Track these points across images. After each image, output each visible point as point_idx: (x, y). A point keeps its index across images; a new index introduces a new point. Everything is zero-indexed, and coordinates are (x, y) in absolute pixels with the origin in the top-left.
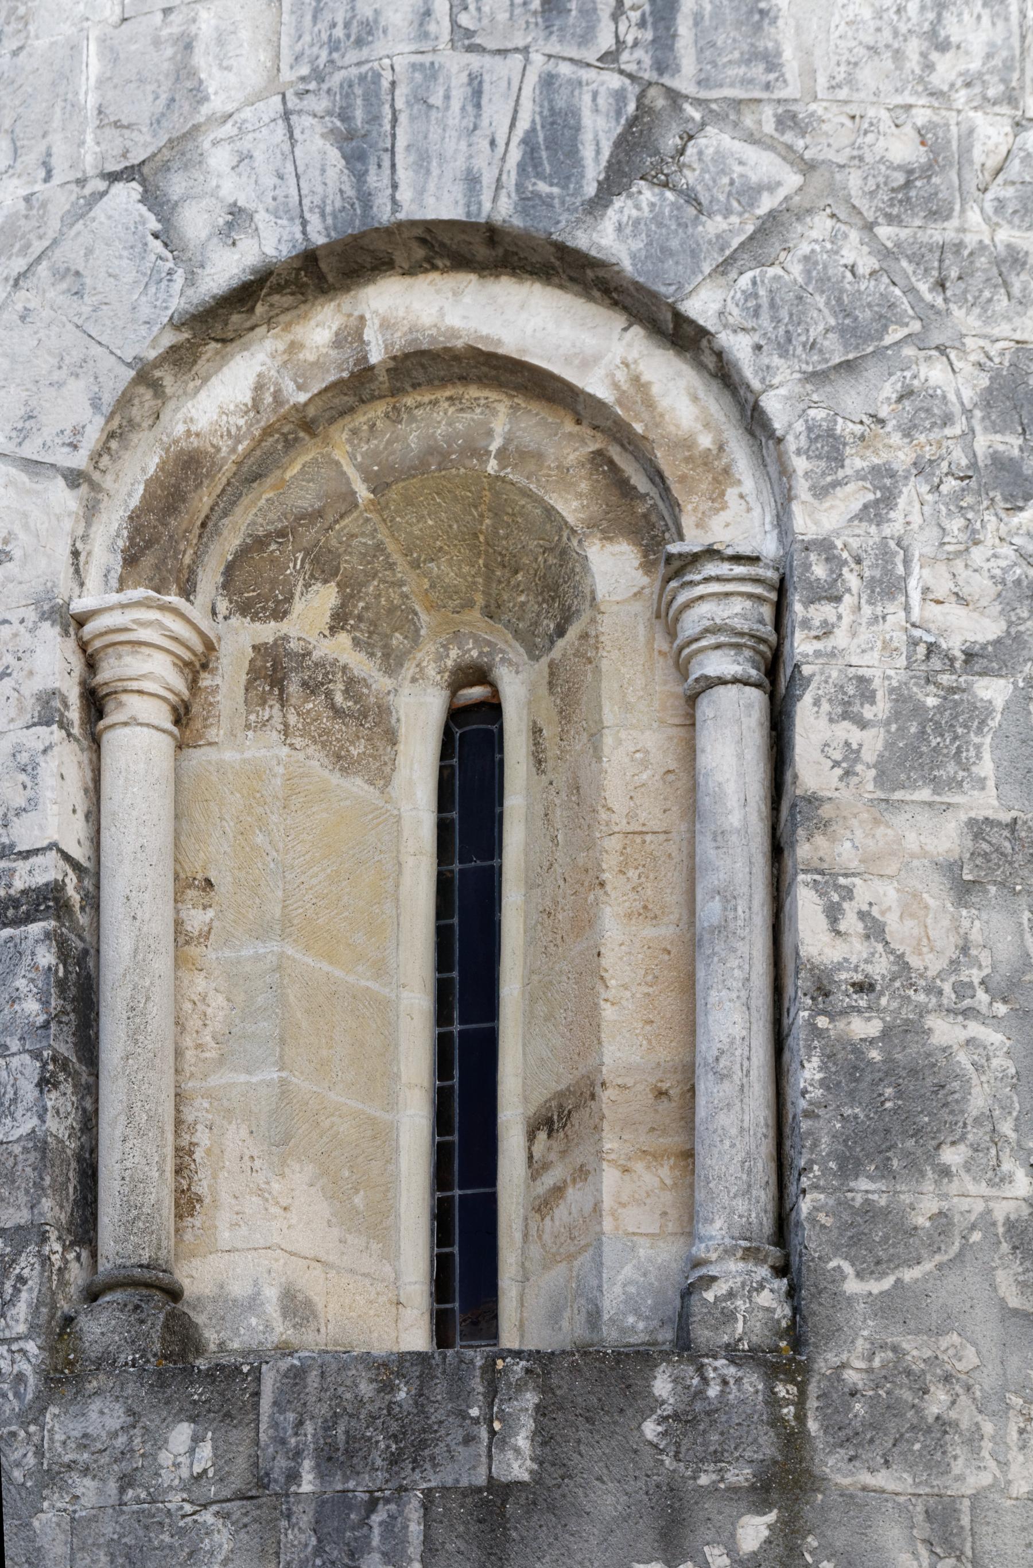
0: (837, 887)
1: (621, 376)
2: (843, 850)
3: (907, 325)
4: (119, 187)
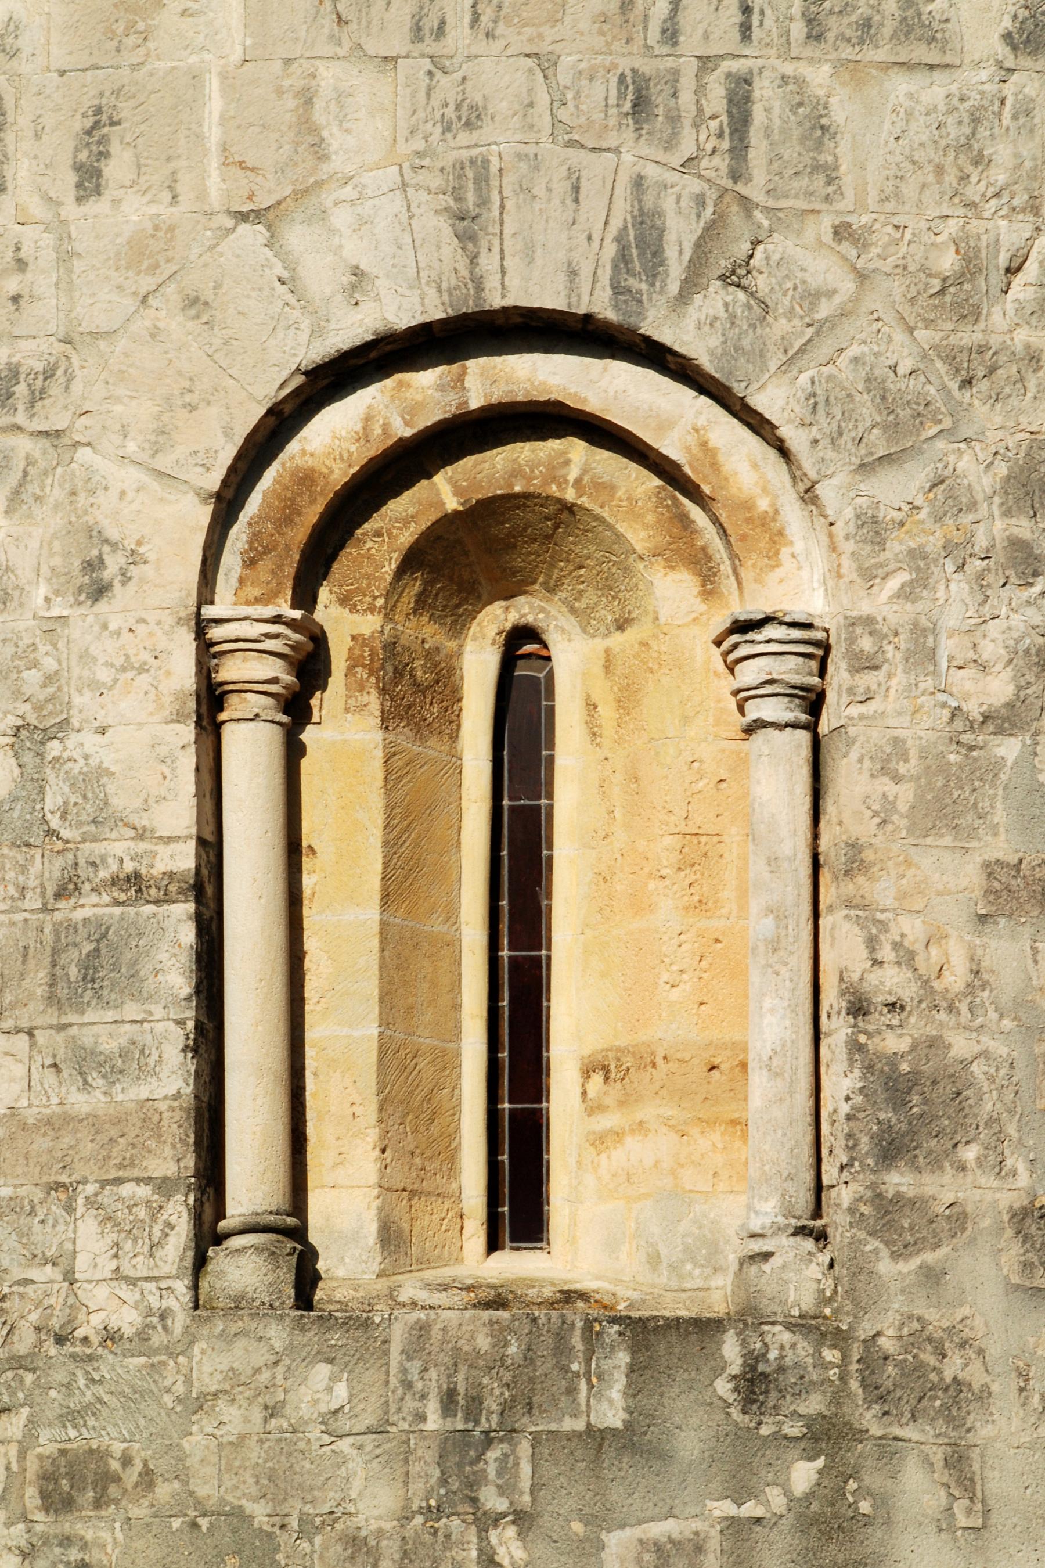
0: (876, 922)
1: (691, 440)
2: (882, 890)
3: (940, 421)
4: (244, 228)
